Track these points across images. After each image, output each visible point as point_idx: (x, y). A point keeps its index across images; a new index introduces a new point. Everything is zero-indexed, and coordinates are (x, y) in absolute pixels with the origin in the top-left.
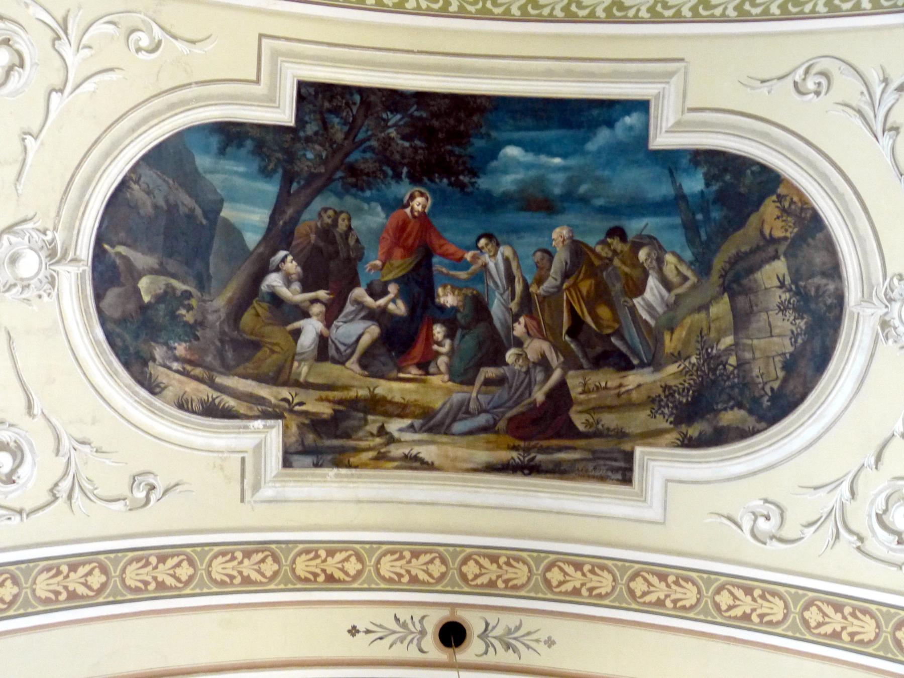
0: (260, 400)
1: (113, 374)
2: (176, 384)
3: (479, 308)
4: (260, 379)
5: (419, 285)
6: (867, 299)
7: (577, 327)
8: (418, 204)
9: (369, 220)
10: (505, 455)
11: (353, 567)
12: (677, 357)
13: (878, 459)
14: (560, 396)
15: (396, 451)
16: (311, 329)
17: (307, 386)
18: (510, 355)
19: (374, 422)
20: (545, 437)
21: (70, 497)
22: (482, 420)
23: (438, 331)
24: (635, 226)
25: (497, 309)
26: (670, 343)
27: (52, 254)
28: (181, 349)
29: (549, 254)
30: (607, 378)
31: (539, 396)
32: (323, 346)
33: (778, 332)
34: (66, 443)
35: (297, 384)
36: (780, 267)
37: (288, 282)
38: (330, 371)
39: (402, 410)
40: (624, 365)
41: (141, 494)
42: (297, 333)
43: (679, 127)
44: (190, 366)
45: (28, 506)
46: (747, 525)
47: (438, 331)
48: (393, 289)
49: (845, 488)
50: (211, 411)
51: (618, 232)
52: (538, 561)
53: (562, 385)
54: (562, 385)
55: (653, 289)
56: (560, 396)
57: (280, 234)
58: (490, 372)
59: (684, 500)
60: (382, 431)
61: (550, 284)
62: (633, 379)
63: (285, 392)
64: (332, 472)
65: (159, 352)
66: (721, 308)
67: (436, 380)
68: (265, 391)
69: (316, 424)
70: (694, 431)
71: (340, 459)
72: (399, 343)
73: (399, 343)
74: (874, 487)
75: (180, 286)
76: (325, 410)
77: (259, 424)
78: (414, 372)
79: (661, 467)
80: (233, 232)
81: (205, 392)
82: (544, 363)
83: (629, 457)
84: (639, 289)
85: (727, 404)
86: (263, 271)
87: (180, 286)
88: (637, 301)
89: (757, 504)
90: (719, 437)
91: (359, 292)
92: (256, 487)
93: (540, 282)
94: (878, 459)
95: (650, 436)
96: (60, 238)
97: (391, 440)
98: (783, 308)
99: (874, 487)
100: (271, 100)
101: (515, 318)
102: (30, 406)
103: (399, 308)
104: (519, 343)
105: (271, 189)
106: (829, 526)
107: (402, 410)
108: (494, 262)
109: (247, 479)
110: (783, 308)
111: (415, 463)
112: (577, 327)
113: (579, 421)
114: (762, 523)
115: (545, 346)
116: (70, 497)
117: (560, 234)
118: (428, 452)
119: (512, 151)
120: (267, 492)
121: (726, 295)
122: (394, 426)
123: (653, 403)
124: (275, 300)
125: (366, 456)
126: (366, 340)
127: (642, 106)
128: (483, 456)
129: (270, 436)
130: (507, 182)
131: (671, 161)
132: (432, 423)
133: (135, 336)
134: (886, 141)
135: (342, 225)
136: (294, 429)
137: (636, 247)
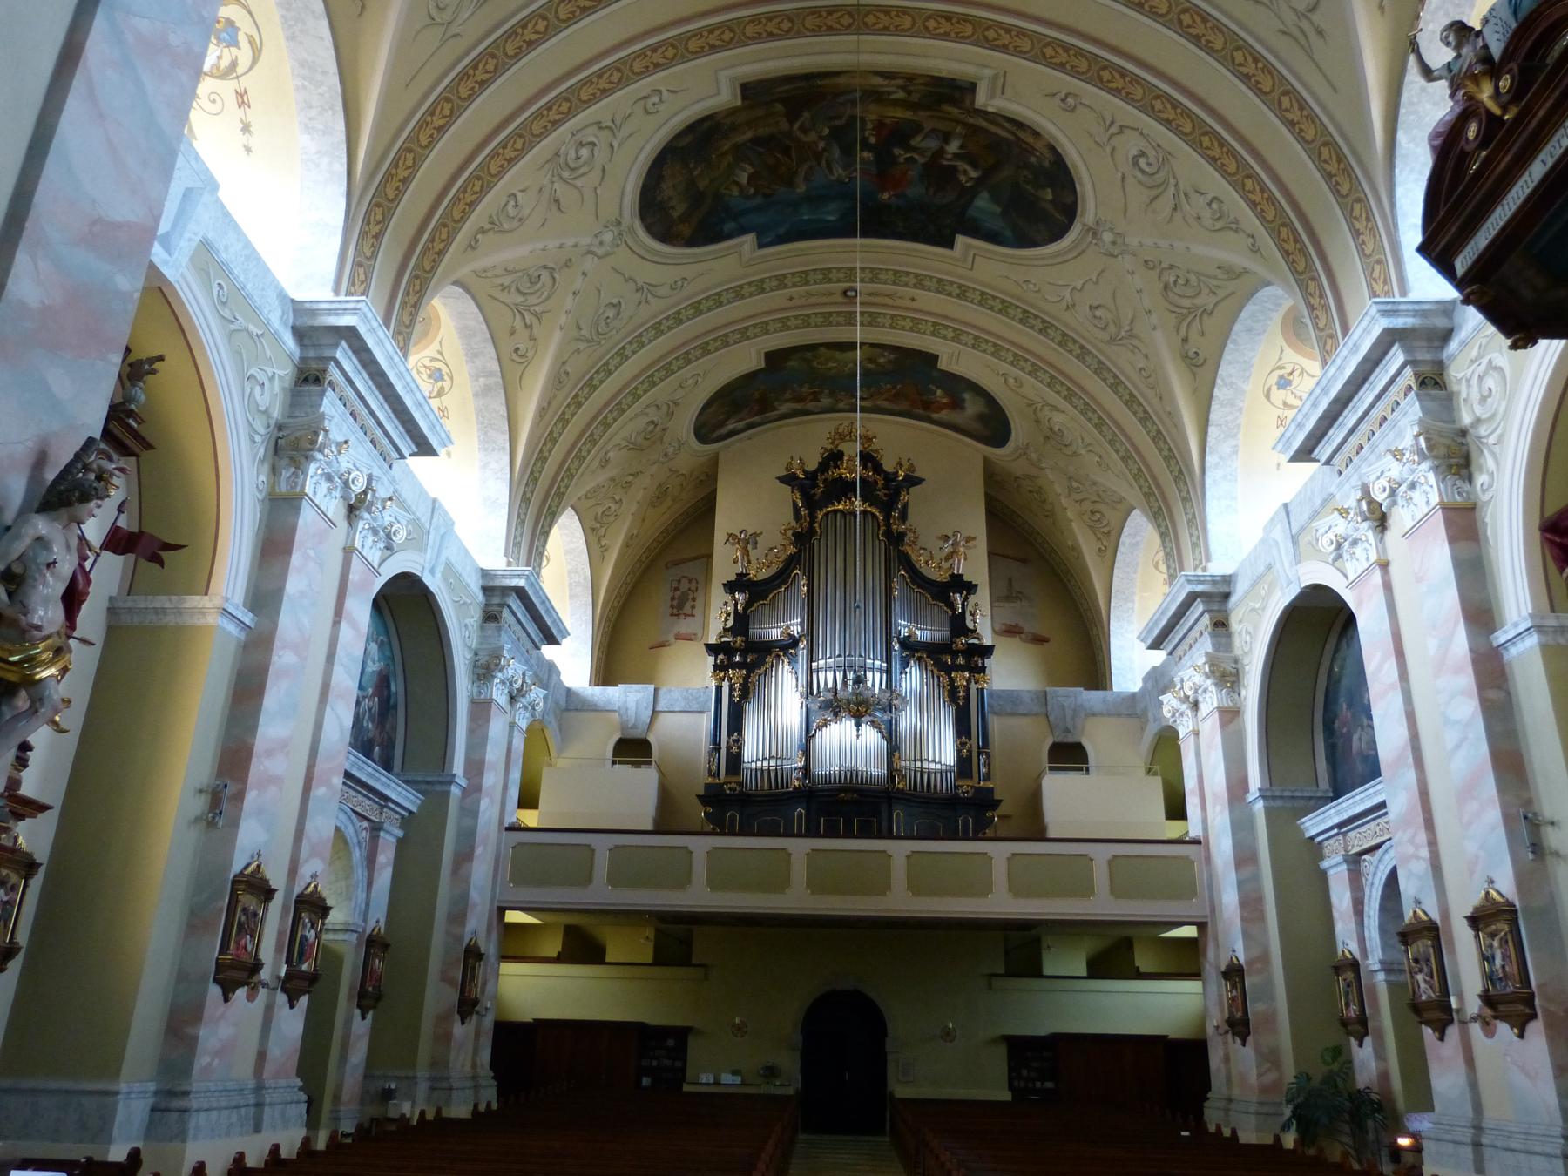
0: (986, 120)
1: (1075, 166)
2: (1039, 145)
3: (848, 152)
4: (986, 131)
5: (884, 160)
6: (631, 230)
7: (786, 151)
8: (886, 196)
9: (915, 191)
10: (827, 81)
11: (932, 24)
12: (724, 154)
13: (604, 170)
14: (792, 116)
15: (900, 82)
16: (953, 147)
17: (958, 122)
18: (826, 131)
19: (915, 97)
20: (802, 94)
21: (1112, 123)
22: (842, 99)
23: (872, 140)
24: (759, 200)
25: (836, 153)
26: (730, 158)
27: (1095, 234)
28: (1033, 160)
29: (806, 179)
30: (762, 131)
31: (806, 115)
32: (946, 137)
33: (669, 190)
34: (1108, 150)
35: (965, 124)
36: (675, 214)
37: (965, 172)
38: (943, 126)
39: (896, 103)
40: (756, 141)
41: (1070, 100)
42: (961, 147)
43: (741, 244)
44: (1031, 150)
45: (1136, 134)
46: (665, 93)
47: (872, 140)
48: (901, 160)
49: (615, 144)
50: (1021, 125)
51: (765, 196)
52: (799, 32)
53: (791, 122)
54: (791, 122)
55: (743, 178)
56: (792, 116)
57: (970, 194)
58: (837, 123)
59: (706, 88)
60: (909, 93)
61: (806, 167)
62: (749, 135)
63: (971, 121)
64: (944, 74)
65: (1047, 164)
66: (702, 184)
67: (874, 117)
68: (985, 124)
69: (954, 102)
70: (707, 125)
71: (938, 81)
72: (899, 135)
73: (899, 135)
74: (601, 155)
75: (1029, 188)
76: (947, 108)
77: (990, 109)
78: (888, 121)
79: (725, 97)
80: (995, 199)
81: (1021, 134)
82: (804, 130)
83: (744, 98)
84: (750, 178)
85: (695, 145)
86: (979, 182)
87: (1029, 188)
88: (751, 170)
89: (661, 108)
90: (691, 128)
91: (922, 160)
92: (995, 77)
93: (811, 168)
94: (604, 170)
95: (733, 111)
96: (1089, 238)
97: (903, 88)
98: (670, 198)
99: (601, 155)
100: (969, 247)
101: (824, 149)
102: (1123, 178)
103: (897, 151)
104: (821, 138)
105: (971, 212)
106: (618, 122)
107: (896, 103)
108: (839, 172)
109: (1000, 84)
110: (670, 198)
111: (888, 75)
112: (786, 151)
113: (779, 107)
114: (656, 99)
115: (805, 139)
116: (1112, 123)
117: (802, 188)
118: (878, 81)
119: (831, 218)
120: (988, 72)
121: (1007, 1096)
122: (901, 95)
123: (734, 128)
124: (975, 166)
125: (921, 81)
126: (919, 138)
127: (761, 246)
128: (841, 80)
129: (981, 99)
130: (833, 206)
131: (743, 231)
132: (876, 96)
133: (1059, 175)
134: (640, 284)
135: (931, 191)
136: (968, 102)
137: (755, 194)
